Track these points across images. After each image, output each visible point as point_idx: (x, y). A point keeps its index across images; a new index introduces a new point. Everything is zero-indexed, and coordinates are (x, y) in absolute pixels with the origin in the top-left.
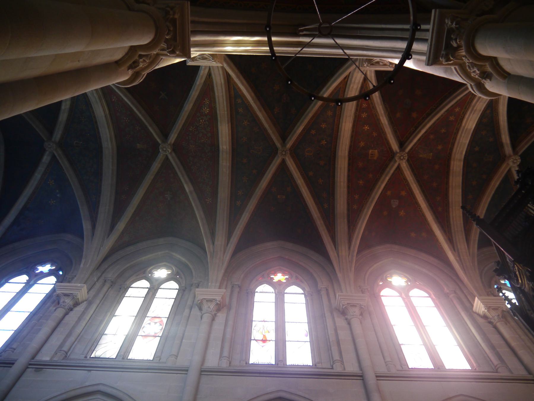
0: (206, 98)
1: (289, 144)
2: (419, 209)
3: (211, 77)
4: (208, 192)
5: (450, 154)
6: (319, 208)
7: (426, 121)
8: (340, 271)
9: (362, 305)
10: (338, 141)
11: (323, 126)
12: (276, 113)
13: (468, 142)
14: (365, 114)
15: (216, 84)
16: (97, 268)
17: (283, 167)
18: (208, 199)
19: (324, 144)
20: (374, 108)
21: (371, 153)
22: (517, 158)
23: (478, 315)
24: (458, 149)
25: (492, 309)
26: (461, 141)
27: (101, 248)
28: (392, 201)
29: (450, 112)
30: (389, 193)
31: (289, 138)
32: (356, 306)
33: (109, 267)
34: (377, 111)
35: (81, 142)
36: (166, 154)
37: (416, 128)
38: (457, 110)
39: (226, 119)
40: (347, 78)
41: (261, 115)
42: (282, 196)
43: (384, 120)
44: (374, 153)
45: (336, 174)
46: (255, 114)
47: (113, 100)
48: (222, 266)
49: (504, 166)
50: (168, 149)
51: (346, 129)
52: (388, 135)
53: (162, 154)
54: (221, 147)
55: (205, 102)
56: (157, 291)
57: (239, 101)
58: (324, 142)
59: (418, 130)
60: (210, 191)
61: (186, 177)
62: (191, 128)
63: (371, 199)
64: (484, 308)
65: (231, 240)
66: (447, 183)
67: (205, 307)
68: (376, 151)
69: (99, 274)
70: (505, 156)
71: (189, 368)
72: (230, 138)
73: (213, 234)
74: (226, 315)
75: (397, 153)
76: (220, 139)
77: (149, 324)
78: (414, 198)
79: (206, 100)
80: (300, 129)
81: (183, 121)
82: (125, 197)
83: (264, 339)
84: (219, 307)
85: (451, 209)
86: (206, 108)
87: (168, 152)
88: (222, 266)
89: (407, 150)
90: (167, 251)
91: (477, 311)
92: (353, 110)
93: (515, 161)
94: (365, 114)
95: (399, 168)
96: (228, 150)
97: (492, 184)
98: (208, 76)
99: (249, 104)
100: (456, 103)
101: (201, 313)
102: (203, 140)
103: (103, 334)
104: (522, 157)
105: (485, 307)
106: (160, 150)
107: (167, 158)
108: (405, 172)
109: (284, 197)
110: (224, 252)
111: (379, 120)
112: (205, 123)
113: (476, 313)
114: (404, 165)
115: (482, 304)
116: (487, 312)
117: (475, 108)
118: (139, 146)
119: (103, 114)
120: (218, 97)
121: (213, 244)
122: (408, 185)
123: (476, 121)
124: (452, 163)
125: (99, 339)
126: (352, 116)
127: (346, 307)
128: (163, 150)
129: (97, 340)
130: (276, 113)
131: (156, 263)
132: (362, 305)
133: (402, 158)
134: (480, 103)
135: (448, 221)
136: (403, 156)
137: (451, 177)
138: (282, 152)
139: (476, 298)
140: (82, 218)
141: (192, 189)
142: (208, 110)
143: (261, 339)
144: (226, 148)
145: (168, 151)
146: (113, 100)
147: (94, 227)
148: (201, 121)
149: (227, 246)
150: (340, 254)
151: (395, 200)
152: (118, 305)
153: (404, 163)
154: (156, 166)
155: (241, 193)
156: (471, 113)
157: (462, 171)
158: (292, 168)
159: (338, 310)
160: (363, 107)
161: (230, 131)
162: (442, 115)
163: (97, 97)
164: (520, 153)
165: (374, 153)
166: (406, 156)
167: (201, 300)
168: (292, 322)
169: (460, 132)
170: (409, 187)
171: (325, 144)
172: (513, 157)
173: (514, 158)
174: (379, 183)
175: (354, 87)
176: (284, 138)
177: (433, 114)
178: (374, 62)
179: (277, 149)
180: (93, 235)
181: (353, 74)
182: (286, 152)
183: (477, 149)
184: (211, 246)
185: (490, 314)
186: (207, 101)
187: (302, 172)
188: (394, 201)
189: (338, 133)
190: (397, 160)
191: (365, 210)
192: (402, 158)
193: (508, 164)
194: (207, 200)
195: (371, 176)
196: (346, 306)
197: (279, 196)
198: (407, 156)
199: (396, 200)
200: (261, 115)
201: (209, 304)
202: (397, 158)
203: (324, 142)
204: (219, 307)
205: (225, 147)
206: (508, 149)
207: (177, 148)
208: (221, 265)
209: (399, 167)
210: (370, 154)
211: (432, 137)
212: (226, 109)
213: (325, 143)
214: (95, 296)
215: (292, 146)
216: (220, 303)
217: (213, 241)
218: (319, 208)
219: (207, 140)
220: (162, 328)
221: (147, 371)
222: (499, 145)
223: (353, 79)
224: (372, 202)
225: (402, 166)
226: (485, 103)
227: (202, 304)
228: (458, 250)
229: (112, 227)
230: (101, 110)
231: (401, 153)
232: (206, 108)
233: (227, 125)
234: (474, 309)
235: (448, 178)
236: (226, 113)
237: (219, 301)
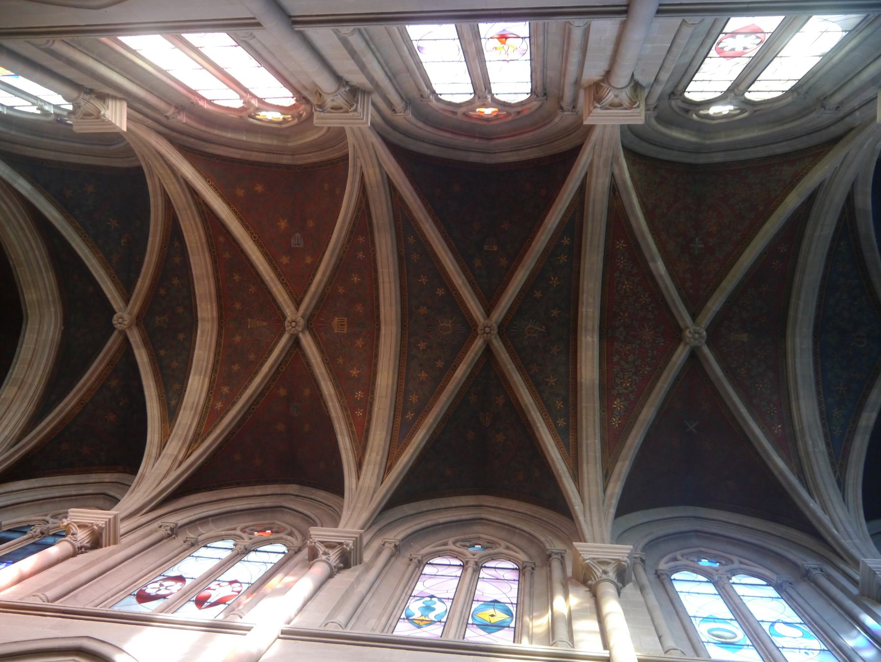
1: (478, 345)
2: (255, 237)
3: (604, 472)
6: (423, 235)
9: (320, 111)
10: (399, 349)
11: (423, 375)
13: (196, 351)
16: (852, 129)
17: (489, 305)
18: (623, 247)
19: (421, 342)
20: (343, 408)
22: (119, 325)
23: (115, 98)
24: (209, 339)
25: (93, 115)
26: (207, 352)
27: (838, 165)
29: (230, 402)
30: (309, 260)
32: (332, 108)
33: (828, 127)
35: (852, 344)
36: (694, 327)
37: (277, 372)
38: (219, 405)
39: (584, 392)
40: (388, 469)
41: (526, 398)
43: (327, 388)
44: (338, 325)
45: (398, 293)
47: (779, 426)
48: (595, 145)
50: (691, 336)
51: (387, 373)
52: (319, 359)
53: (703, 326)
54: (596, 339)
55: (619, 420)
56: (731, 88)
57: (561, 422)
58: (422, 345)
59: (274, 369)
60: (619, 261)
62: (646, 370)
63: (337, 252)
64: (106, 116)
65: (578, 183)
66: (217, 281)
67: (624, 96)
68: (336, 331)
69: (848, 120)
70: (137, 325)
71: (655, 17)
72: (579, 354)
73: (614, 190)
74: (583, 78)
75: (302, 331)
76: (597, 353)
77: (745, 48)
78: (265, 254)
79: (617, 425)
80: (461, 372)
82: (780, 248)
83: (504, 39)
84: (596, 90)
85: (204, 240)
87: (691, 330)
88: (595, 145)
90: (708, 142)
91: (118, 103)
92: (376, 409)
93: (120, 320)
95: (297, 304)
97: (147, 281)
98: (610, 473)
99: (546, 415)
100: (222, 418)
101: (635, 81)
103: (850, 31)
104: (112, 329)
105: (105, 118)
106: (705, 333)
107: (694, 316)
109: (486, 247)
110: (591, 164)
111: (336, 386)
113: (121, 99)
114: (288, 309)
115: (113, 122)
116: (101, 110)
117: (193, 412)
118: (744, 337)
119: (802, 403)
120: (595, 435)
121: (613, 175)
122: (279, 276)
123: (188, 390)
124: (215, 314)
125: (863, 23)
126: (377, 398)
127: (352, 106)
128: (699, 333)
129: (868, 23)
131: (727, 123)
132: (320, 111)
133: (293, 324)
136: (293, 327)
137: (213, 291)
139: (125, 130)
140: (871, 215)
141: (651, 265)
142: (615, 404)
143: (509, 39)
144: (586, 338)
145: (690, 332)
146: (779, 426)
147: (850, 199)
148: (628, 384)
149: (586, 174)
150: (377, 170)
152: (813, 69)
153: (289, 314)
154: (715, 304)
156: (198, 403)
157: (198, 303)
159: (365, 92)
160: (361, 410)
163: (808, 438)
164: (116, 333)
165: (338, 325)
166: (288, 326)
167: (632, 108)
168: (449, 62)
169: (210, 366)
173: (123, 325)
174: (325, 279)
176: (488, 351)
177: (254, 397)
178: (339, 547)
179: (501, 333)
180: (853, 185)
181: (377, 483)
182: (483, 331)
183: (181, 336)
184: (616, 172)
185: (95, 106)
186: (615, 422)
187: (456, 294)
188: (298, 244)
192: (293, 324)
193: (130, 314)
194: (624, 245)
196: (350, 110)
197: (495, 248)
198: (286, 327)
199: (296, 246)
200: (526, 398)
201: (617, 100)
202: (302, 322)
203: (422, 345)
204: (597, 93)
205: (589, 339)
206: (135, 338)
207: (675, 334)
208: (596, 147)
209: (297, 304)
211: (252, 357)
213: (419, 345)
214: (862, 88)
215: (472, 342)
216: (595, 102)
217: (613, 179)
220: (718, 44)
221: (750, 5)
222: (151, 343)
223: (376, 471)
224: (334, 249)
225: (293, 308)
227: (630, 99)
228: (178, 181)
229: (812, 198)
230: (803, 411)
232: (619, 408)
233: (583, 380)
234: (125, 105)
236: (584, 404)
237: (595, 107)
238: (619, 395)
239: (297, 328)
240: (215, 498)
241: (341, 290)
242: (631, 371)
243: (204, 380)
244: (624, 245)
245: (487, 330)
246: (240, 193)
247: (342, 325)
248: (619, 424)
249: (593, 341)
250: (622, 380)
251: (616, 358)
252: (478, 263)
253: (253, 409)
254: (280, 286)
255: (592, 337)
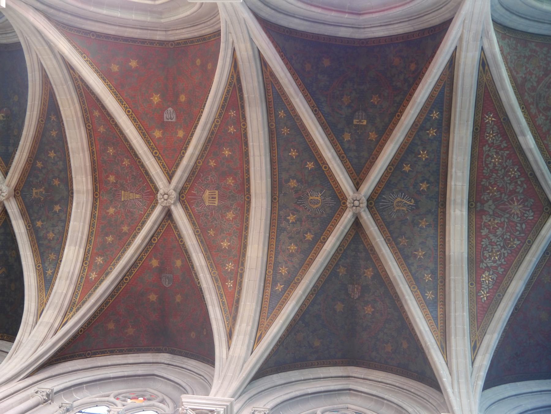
0: (485, 300)
2: (129, 112)
4: (491, 132)
5: (95, 199)
7: (136, 256)
8: (244, 19)
11: (293, 248)
12: (371, 269)
14: (228, 269)
15: (464, 336)
18: (492, 121)
19: (291, 215)
20: (215, 280)
21: (215, 201)
24: (84, 211)
26: (82, 224)
28: (174, 120)
29: (104, 272)
31: (348, 227)
34: (210, 273)
37: (150, 243)
38: (93, 276)
39: (452, 265)
40: (258, 339)
42: (359, 123)
46: (403, 271)
49: (14, 183)
52: (191, 231)
54: (465, 213)
55: (487, 293)
57: (429, 295)
58: (291, 218)
61: (531, 159)
62: (515, 244)
63: (209, 126)
65: (448, 58)
68: (207, 204)
72: (447, 227)
75: (174, 204)
79: (485, 298)
81: (528, 258)
85: (80, 114)
86: (487, 281)
89: (158, 210)
94: (228, 269)
96: (452, 206)
102: (496, 222)
108: (159, 170)
109: (355, 122)
110: (461, 39)
112: (490, 254)
117: (68, 281)
122: (152, 149)
124: (90, 187)
126: (248, 270)
130: (371, 269)
134: (62, 293)
135: (80, 96)
137: (88, 164)
138: (358, 200)
141: (521, 139)
144: (455, 211)
148: (496, 258)
150: (249, 45)
151: (170, 120)
155: (432, 132)
158: (341, 176)
161: (447, 239)
162: (114, 265)
169: (85, 237)
170: (150, 145)
171: (289, 216)
172: (4, 198)
174: (197, 153)
175: (246, 324)
177: (128, 267)
182: (352, 205)
183: (57, 208)
184: (486, 46)
186: (484, 295)
189: (271, 210)
190: (174, 193)
191: (215, 110)
193: (8, 186)
194: (493, 119)
195: (212, 164)
197: (365, 123)
199: (168, 120)
202: (174, 195)
203: (291, 218)
205: (458, 212)
209: (170, 177)
210: (217, 198)
212: (452, 285)
213: (289, 218)
218: (294, 110)
219: (489, 223)
224: (206, 124)
225: (165, 181)
226: (55, 292)
231: (168, 205)
232: (487, 281)
233: (452, 254)
235: (93, 162)
236: (452, 277)
238: (488, 268)
239: (169, 200)
240: (89, 366)
241: (212, 164)
242: (499, 245)
243: (79, 251)
244: (493, 119)
245: (357, 203)
246: (115, 68)
247: (213, 198)
248: (487, 297)
249: (462, 215)
250: (490, 254)
251: (484, 232)
252: (347, 137)
253: (126, 279)
254: (153, 159)
255: (461, 211)
